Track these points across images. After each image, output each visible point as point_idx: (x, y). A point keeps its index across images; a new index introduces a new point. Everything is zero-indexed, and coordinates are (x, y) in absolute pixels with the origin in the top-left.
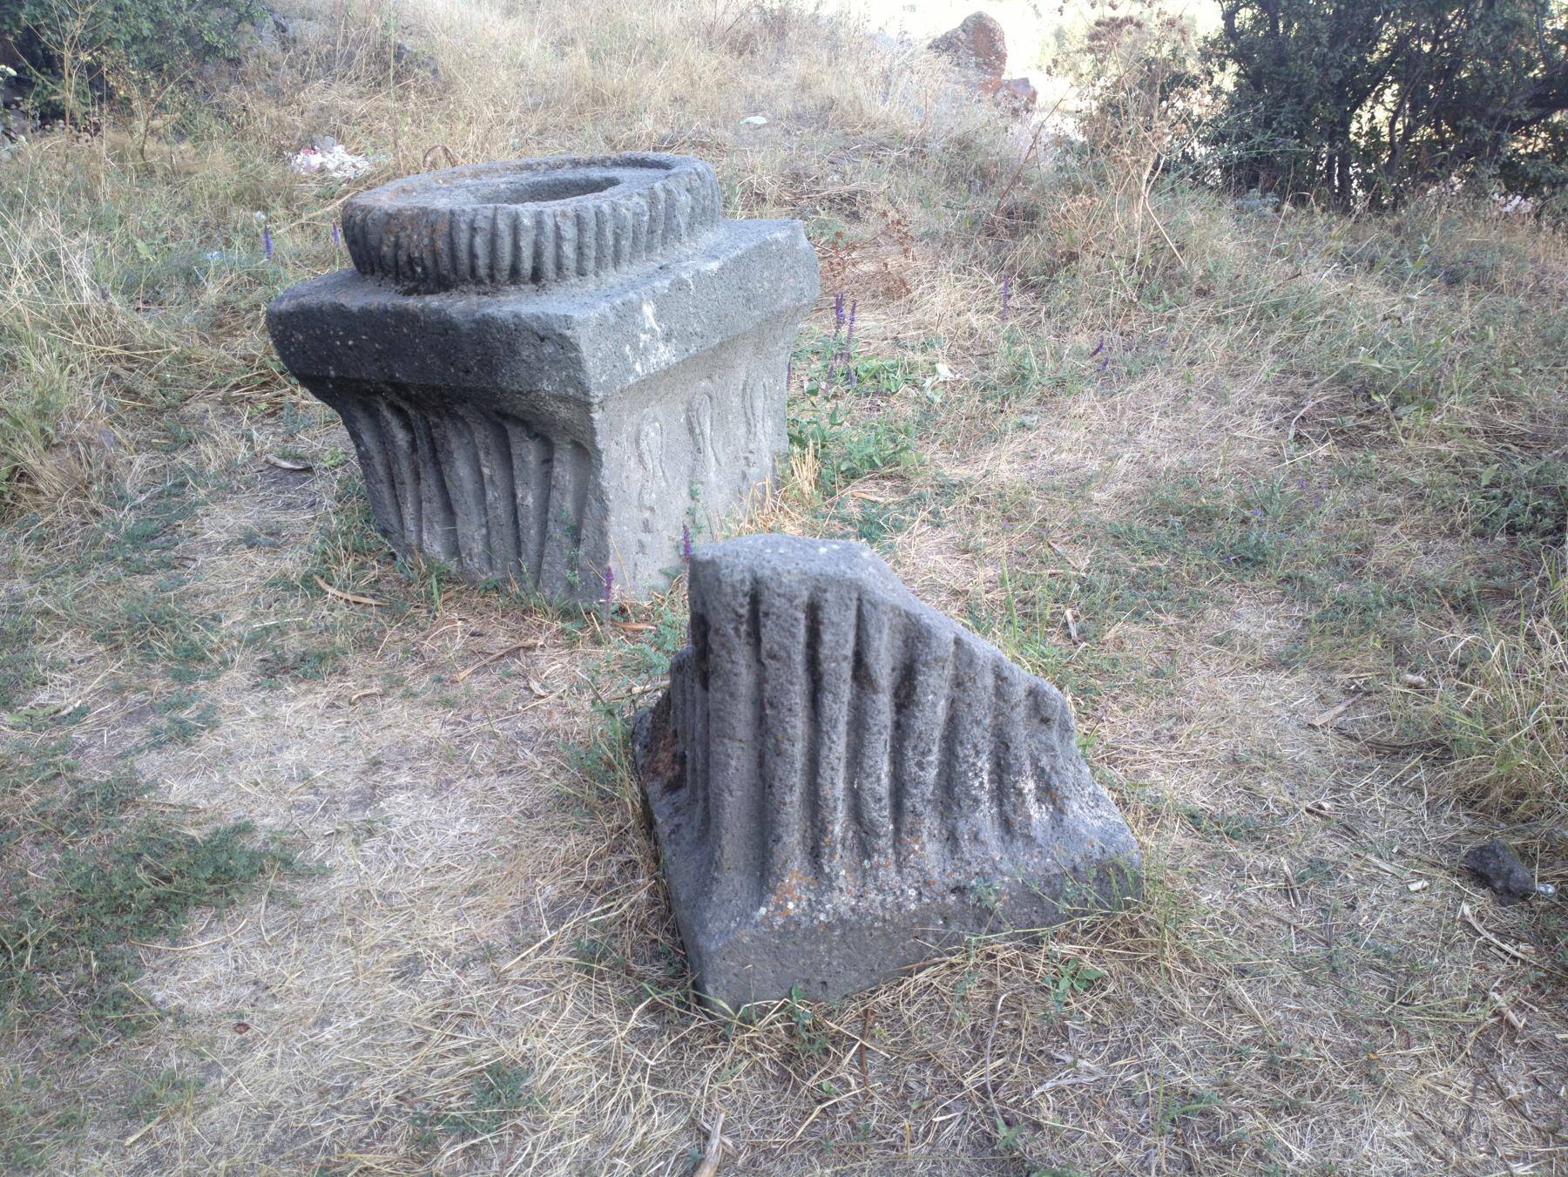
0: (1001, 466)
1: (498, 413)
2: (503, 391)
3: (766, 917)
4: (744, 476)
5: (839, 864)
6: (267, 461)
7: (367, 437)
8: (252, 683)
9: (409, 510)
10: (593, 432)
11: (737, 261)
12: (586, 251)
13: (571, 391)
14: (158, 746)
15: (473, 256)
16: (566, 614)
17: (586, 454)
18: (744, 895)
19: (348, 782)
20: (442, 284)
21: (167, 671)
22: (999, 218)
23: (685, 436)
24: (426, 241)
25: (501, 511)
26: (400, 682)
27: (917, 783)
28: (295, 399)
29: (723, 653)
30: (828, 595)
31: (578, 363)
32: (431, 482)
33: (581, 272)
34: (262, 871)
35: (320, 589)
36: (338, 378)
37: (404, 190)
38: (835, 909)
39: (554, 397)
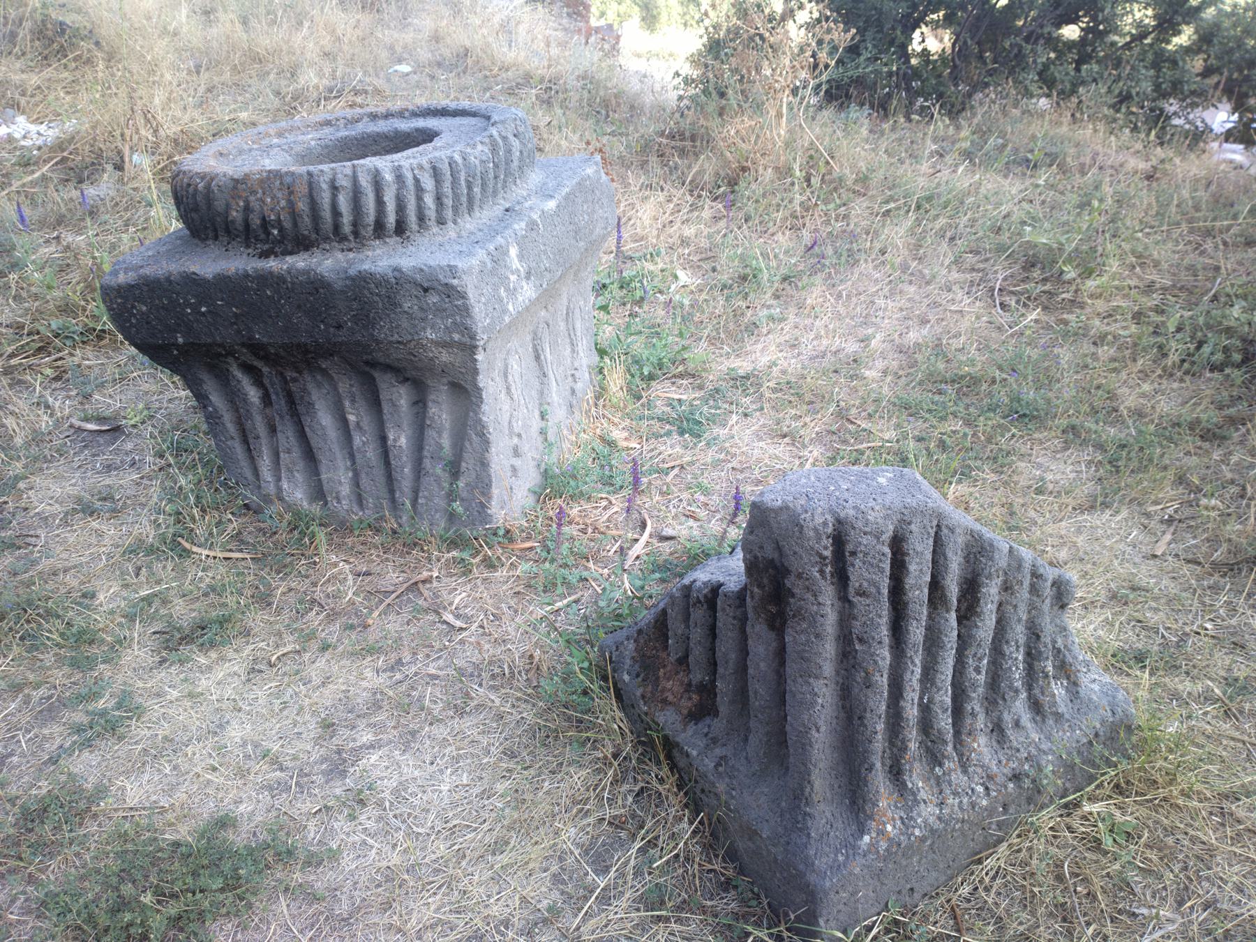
0: (765, 355)
1: (367, 363)
2: (378, 342)
3: (871, 844)
4: (573, 391)
5: (916, 779)
6: (71, 426)
7: (217, 399)
8: (157, 659)
9: (265, 464)
10: (476, 372)
11: (567, 198)
12: (445, 200)
13: (456, 337)
14: (88, 744)
15: (336, 213)
16: (453, 544)
17: (465, 391)
18: (840, 825)
19: (307, 749)
20: (303, 244)
21: (60, 659)
22: (664, 141)
23: (534, 364)
24: (283, 203)
25: (371, 453)
26: (311, 636)
27: (974, 686)
28: (76, 360)
29: (809, 596)
30: (913, 527)
31: (466, 310)
32: (290, 433)
33: (441, 222)
34: (268, 867)
35: (185, 550)
36: (185, 344)
37: (221, 154)
38: (925, 822)
39: (436, 343)
